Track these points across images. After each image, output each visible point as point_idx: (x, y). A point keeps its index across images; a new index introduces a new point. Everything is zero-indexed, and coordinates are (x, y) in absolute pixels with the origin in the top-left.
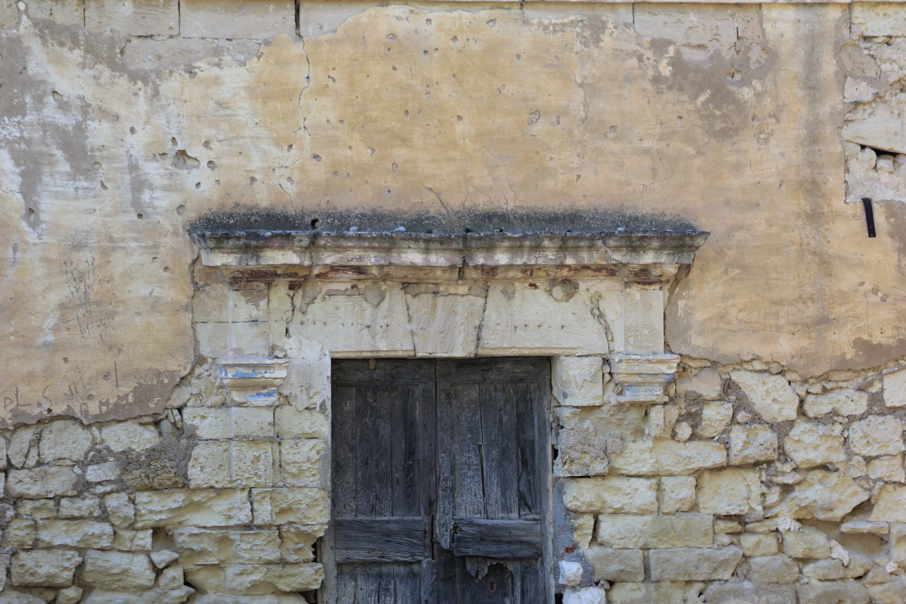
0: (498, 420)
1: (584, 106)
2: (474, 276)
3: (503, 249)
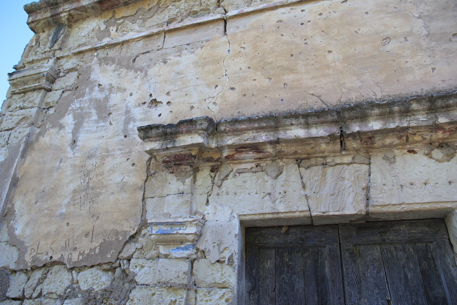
0: (402, 276)
1: (425, 28)
2: (355, 146)
3: (375, 117)
